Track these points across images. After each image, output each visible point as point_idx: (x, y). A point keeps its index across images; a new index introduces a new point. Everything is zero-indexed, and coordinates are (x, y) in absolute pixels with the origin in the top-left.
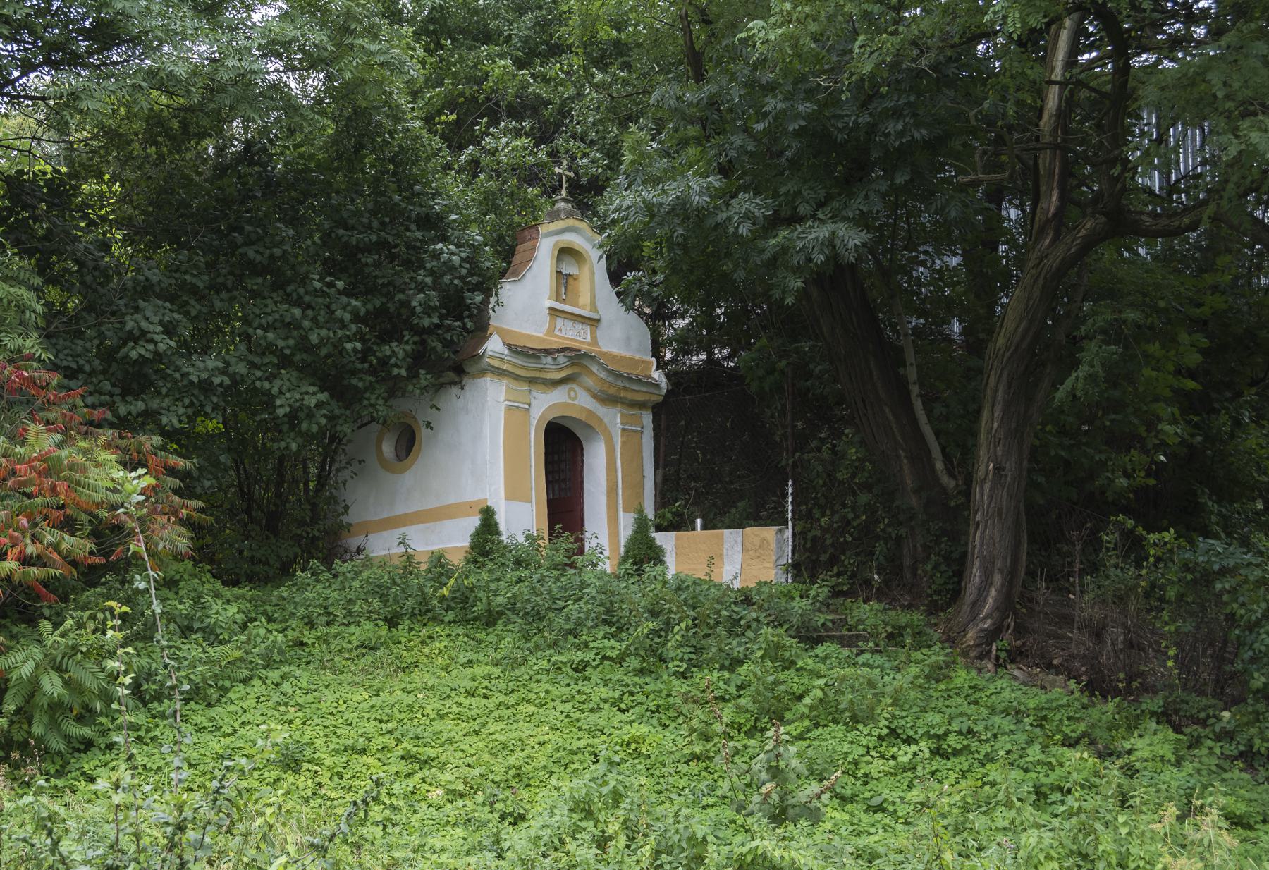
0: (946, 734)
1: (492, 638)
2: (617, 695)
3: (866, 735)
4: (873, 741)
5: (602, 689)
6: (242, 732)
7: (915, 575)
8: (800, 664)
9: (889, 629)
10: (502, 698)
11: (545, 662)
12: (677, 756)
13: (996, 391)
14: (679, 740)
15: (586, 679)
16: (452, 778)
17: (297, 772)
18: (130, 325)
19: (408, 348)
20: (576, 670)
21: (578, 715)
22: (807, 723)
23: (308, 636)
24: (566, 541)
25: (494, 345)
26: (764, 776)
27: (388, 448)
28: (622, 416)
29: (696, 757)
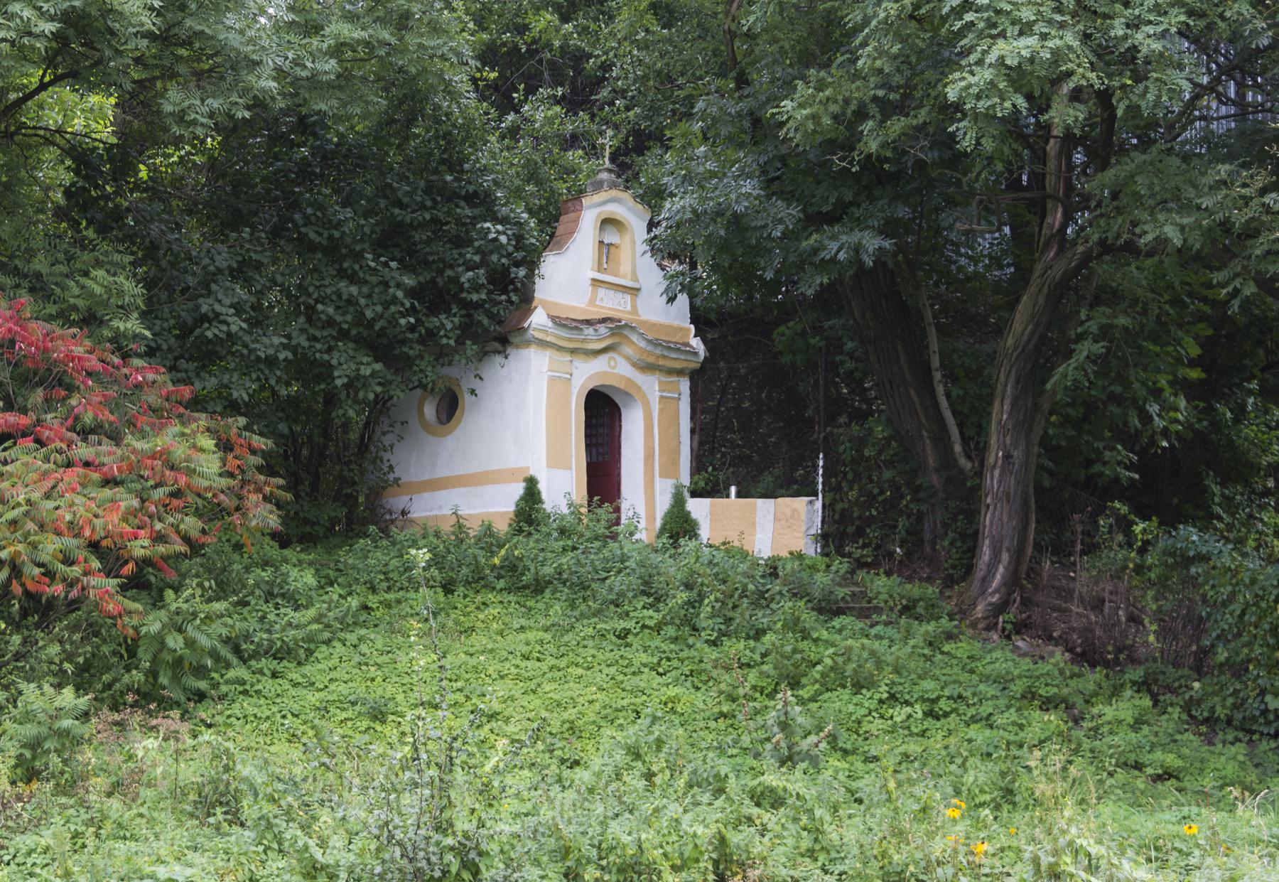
0: (938, 698)
1: (541, 606)
2: (655, 660)
3: (868, 699)
4: (873, 704)
5: (643, 655)
6: (332, 687)
7: (934, 549)
8: (815, 635)
9: (904, 602)
10: (553, 662)
11: (591, 629)
12: (707, 714)
13: (1006, 386)
14: (709, 700)
15: (628, 645)
16: (516, 730)
17: (383, 722)
18: (204, 309)
19: (456, 320)
20: (619, 637)
21: (621, 677)
22: (817, 686)
23: (373, 601)
24: (604, 512)
25: (538, 319)
26: (776, 729)
27: (430, 411)
28: (661, 383)
29: (723, 715)
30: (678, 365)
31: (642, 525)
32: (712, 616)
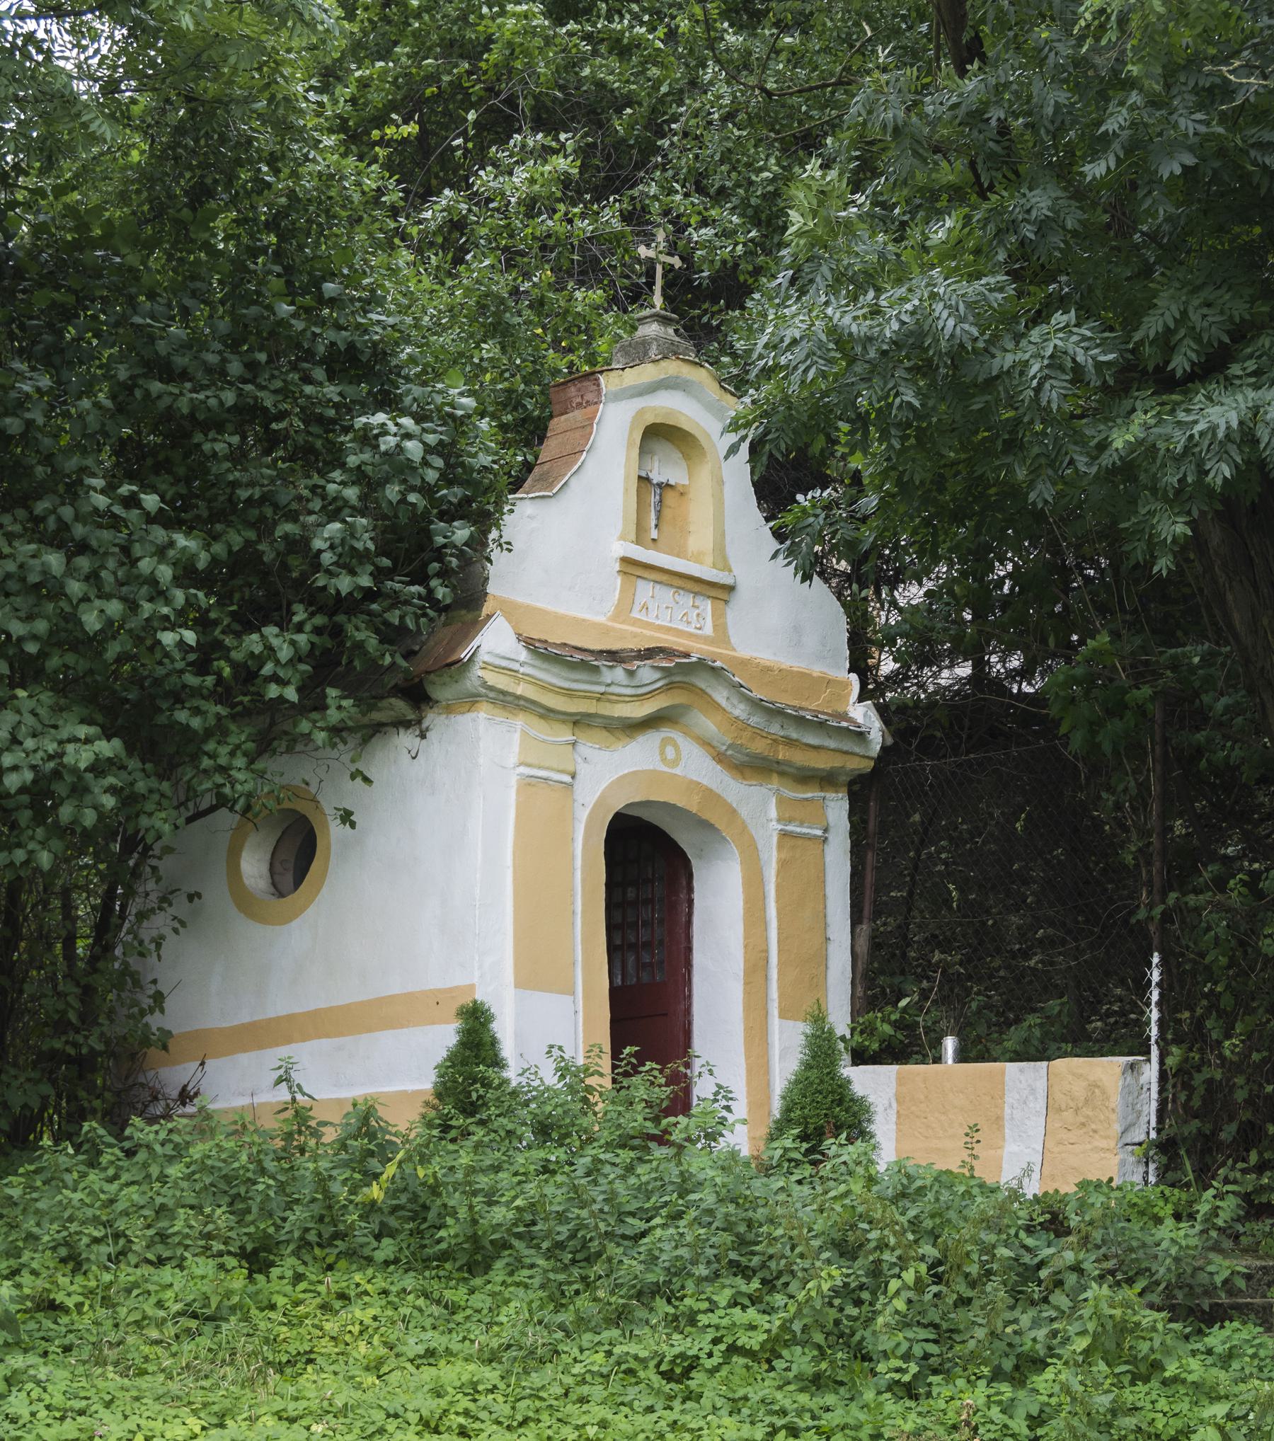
1: (478, 1301)
5: (727, 1421)
8: (1171, 1370)
11: (600, 1357)
15: (690, 1396)
19: (302, 639)
20: (668, 1376)
23: (68, 1290)
28: (781, 802)
30: (822, 762)
31: (741, 1109)
32: (904, 1323)
